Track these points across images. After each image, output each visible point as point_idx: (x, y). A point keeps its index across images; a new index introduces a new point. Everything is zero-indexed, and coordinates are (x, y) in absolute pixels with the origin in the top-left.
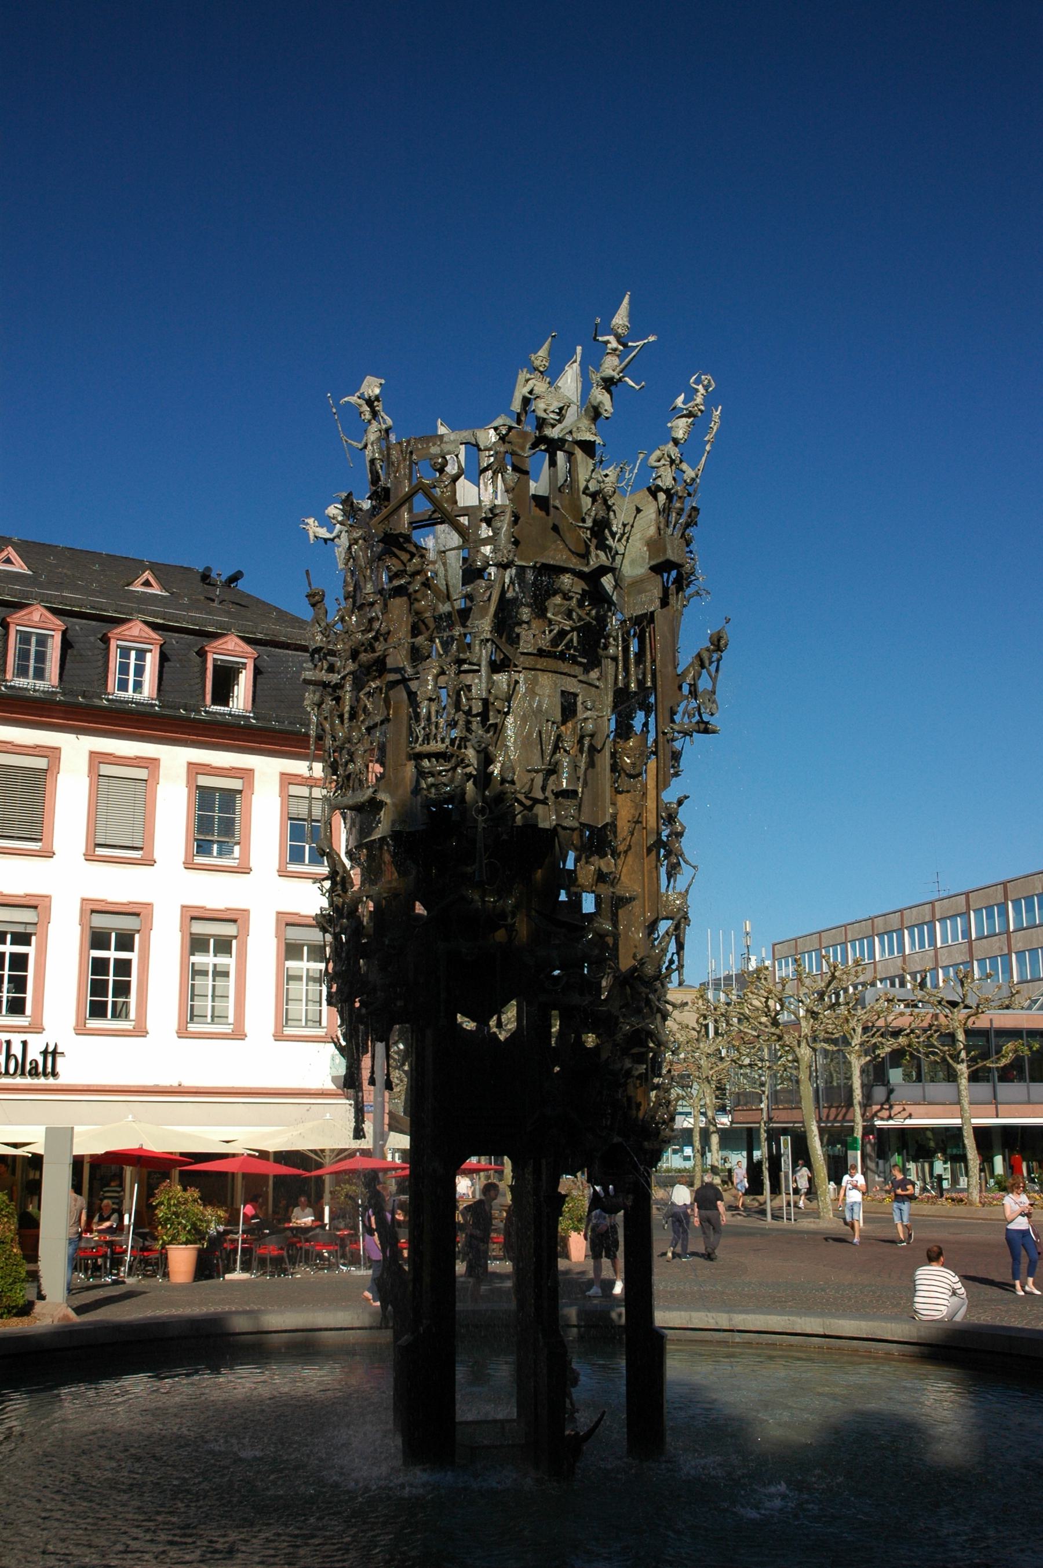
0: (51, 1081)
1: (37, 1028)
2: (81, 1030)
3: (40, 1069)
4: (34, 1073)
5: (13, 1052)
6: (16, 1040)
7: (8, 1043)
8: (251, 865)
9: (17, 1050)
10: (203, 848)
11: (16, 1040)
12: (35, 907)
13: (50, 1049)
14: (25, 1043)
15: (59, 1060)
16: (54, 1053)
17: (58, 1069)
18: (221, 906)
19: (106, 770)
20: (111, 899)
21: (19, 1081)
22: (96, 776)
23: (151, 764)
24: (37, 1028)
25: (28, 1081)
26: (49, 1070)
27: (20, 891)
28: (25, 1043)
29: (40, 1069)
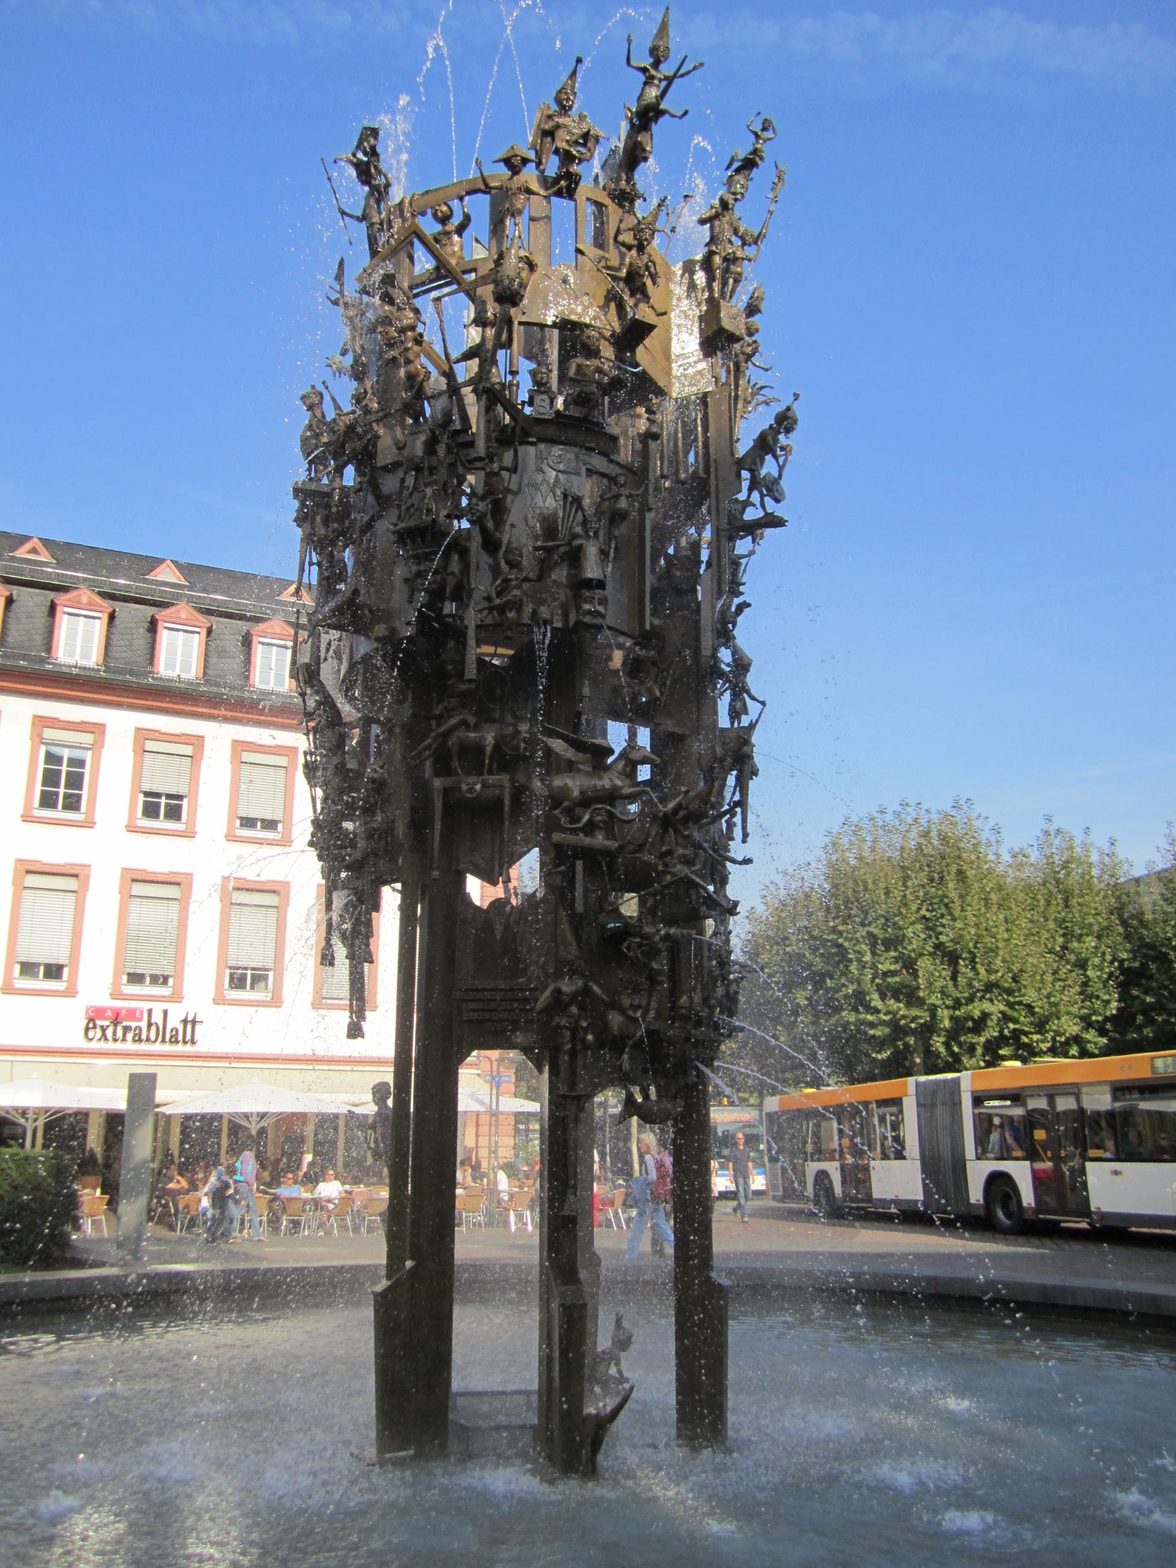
0: (188, 1048)
1: (177, 997)
2: (219, 1000)
3: (180, 1037)
4: (174, 1040)
5: (153, 1021)
6: (158, 1008)
7: (150, 1011)
8: (197, 829)
9: (157, 1018)
10: (48, 801)
11: (158, 1008)
12: (76, 876)
13: (190, 1019)
14: (165, 1012)
15: (197, 1027)
16: (194, 1022)
17: (196, 1037)
18: (61, 861)
19: (150, 745)
20: (151, 869)
21: (158, 1047)
22: (237, 762)
23: (98, 729)
24: (177, 997)
25: (167, 1048)
26: (188, 1037)
27: (164, 869)
28: (165, 1012)
29: (180, 1037)
